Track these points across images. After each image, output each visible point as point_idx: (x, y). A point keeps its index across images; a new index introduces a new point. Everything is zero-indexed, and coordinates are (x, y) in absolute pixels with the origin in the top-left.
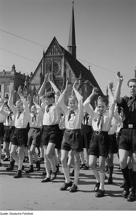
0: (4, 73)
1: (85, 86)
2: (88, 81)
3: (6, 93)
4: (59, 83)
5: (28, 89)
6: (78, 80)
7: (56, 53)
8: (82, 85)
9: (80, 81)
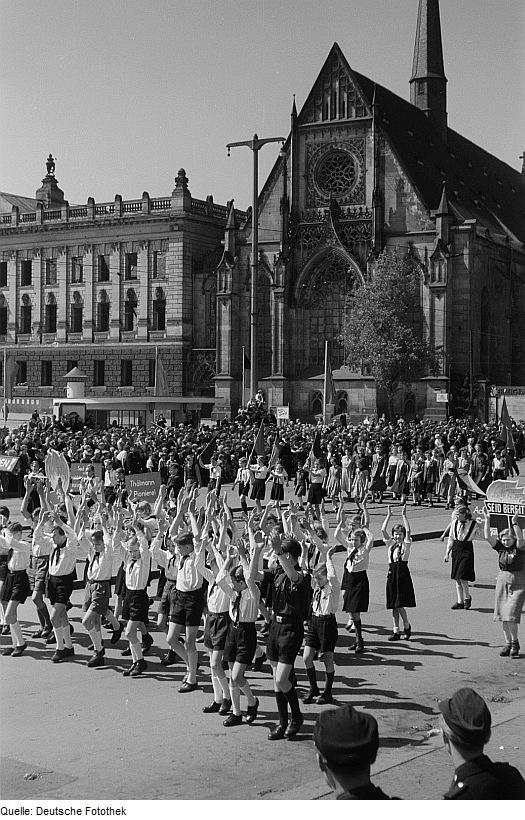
0: (145, 205)
1: (463, 241)
2: (474, 221)
3: (155, 285)
4: (354, 234)
5: (237, 266)
6: (433, 219)
7: (342, 110)
8: (451, 241)
9: (439, 220)
